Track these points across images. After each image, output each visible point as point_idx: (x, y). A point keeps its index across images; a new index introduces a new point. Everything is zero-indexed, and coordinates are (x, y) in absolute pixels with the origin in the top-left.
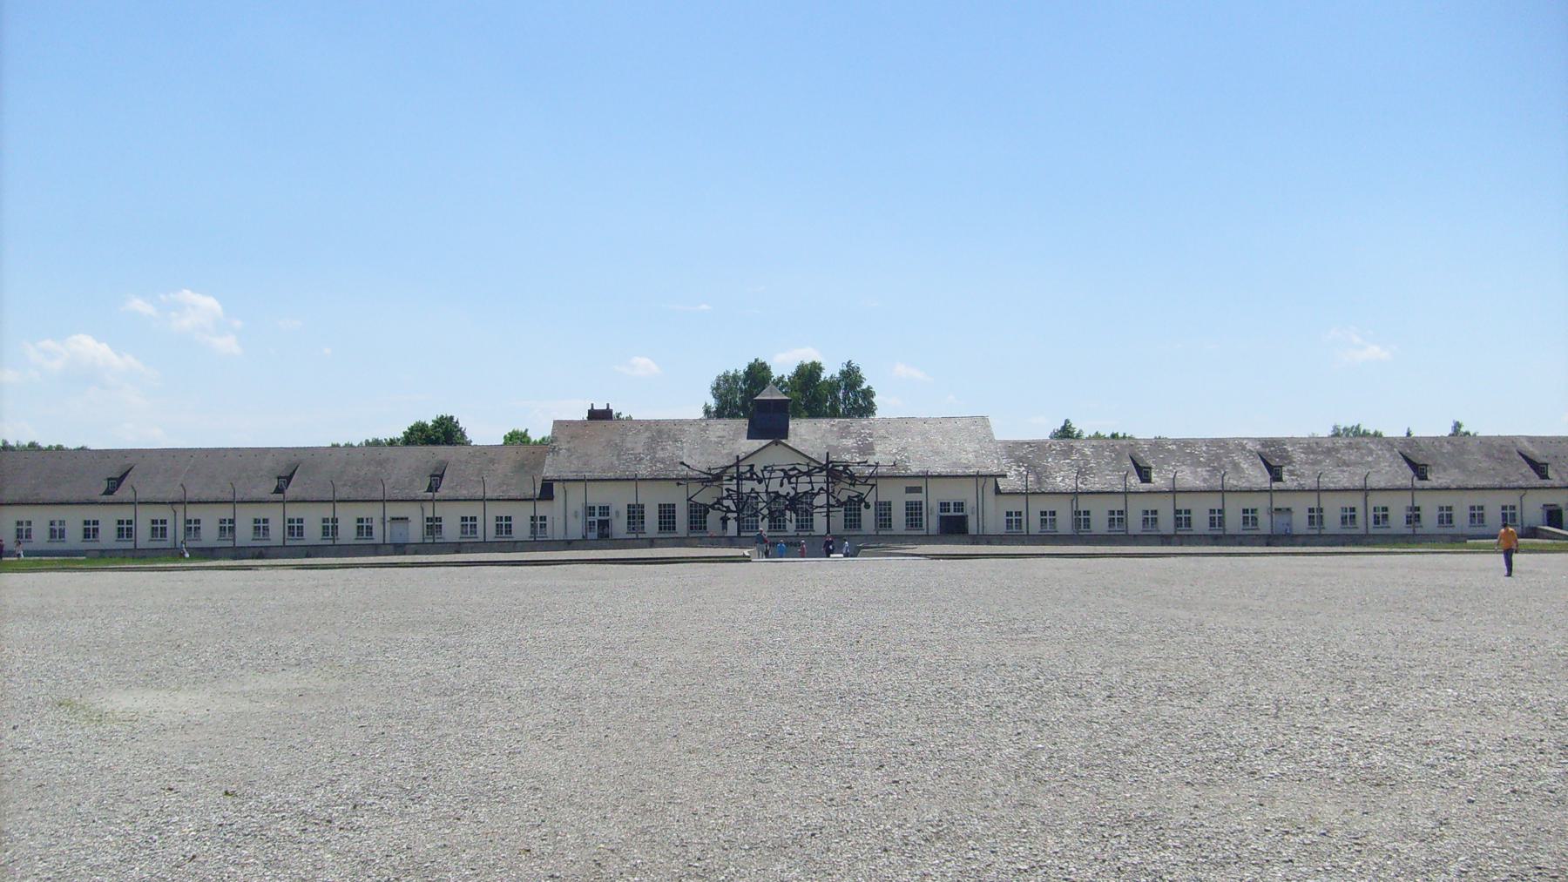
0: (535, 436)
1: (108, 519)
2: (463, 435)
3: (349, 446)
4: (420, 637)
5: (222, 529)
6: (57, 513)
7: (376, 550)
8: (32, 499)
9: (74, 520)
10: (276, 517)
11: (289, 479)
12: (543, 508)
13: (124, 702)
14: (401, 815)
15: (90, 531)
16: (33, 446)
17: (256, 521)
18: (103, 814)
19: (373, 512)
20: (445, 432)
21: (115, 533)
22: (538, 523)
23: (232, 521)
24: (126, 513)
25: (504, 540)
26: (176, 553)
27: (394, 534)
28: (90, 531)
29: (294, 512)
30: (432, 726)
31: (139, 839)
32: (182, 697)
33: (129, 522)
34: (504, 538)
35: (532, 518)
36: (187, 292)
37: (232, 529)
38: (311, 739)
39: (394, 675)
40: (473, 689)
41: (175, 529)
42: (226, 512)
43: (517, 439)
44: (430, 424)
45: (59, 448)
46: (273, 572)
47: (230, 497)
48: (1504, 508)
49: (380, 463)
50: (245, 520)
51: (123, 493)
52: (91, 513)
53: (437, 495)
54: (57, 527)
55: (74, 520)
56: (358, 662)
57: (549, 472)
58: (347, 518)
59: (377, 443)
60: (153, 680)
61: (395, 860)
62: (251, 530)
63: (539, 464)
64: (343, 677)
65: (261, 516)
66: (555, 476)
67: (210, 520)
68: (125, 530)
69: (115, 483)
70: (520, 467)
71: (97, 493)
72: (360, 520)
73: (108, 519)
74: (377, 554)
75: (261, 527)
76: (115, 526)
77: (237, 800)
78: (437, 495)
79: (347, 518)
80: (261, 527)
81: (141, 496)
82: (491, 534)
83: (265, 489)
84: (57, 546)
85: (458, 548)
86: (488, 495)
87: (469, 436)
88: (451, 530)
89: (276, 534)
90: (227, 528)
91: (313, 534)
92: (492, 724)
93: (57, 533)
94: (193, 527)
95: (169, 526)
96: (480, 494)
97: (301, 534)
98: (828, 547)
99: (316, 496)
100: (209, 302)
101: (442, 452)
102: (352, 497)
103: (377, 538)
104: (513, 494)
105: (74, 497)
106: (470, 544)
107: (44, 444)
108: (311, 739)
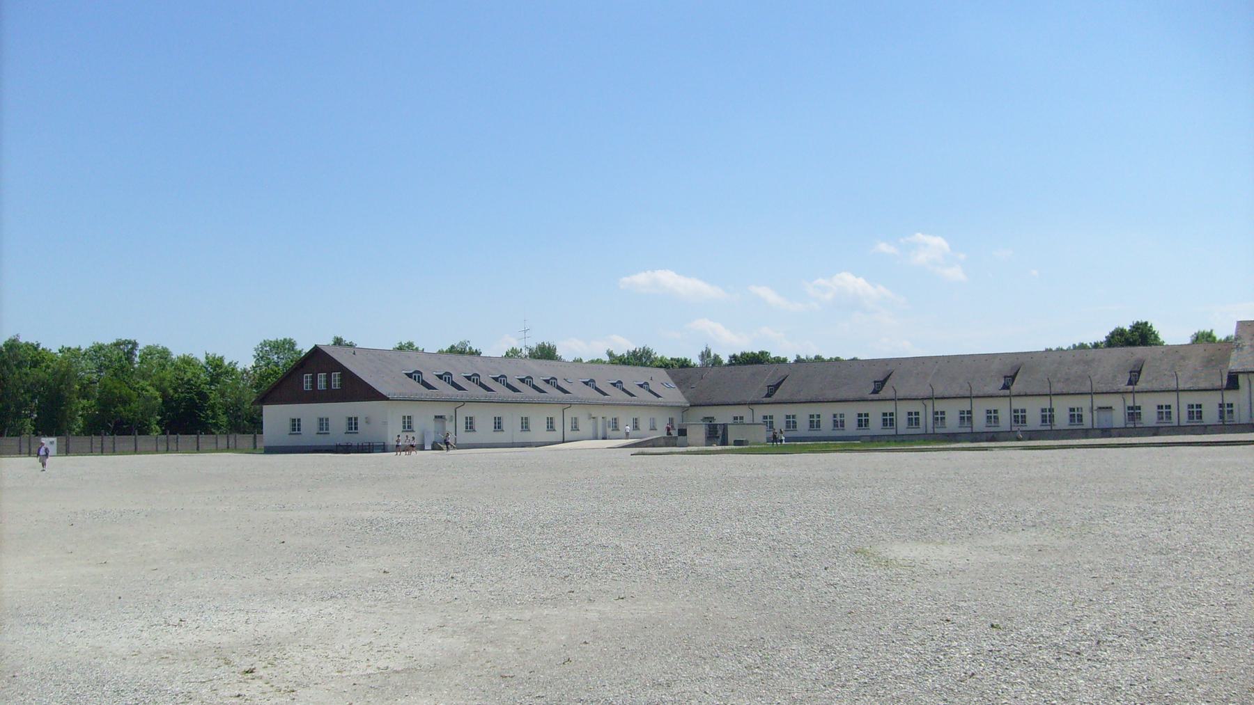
0: (1220, 335)
1: (875, 412)
2: (1156, 337)
3: (1060, 350)
4: (1132, 505)
5: (962, 419)
6: (838, 409)
7: (1086, 433)
8: (821, 398)
9: (850, 413)
10: (1004, 410)
11: (1013, 378)
12: (1230, 397)
13: (902, 551)
14: (1139, 652)
15: (863, 421)
16: (818, 358)
17: (989, 412)
18: (899, 636)
19: (1083, 403)
20: (1141, 335)
21: (808, 424)
22: (1225, 410)
23: (969, 412)
24: (889, 407)
25: (1195, 424)
26: (952, 437)
27: (1102, 420)
28: (863, 421)
29: (1018, 404)
30: (1155, 577)
31: (929, 657)
32: (946, 550)
33: (891, 414)
34: (1195, 422)
35: (1221, 406)
36: (919, 235)
37: (970, 419)
38: (1053, 586)
39: (1114, 535)
40: (1186, 550)
41: (926, 420)
42: (965, 405)
43: (1204, 338)
44: (1127, 328)
45: (837, 359)
46: (1005, 452)
47: (968, 394)
48: (835, 416)
49: (1087, 363)
50: (980, 411)
51: (886, 392)
52: (863, 408)
53: (1137, 388)
54: (838, 419)
55: (850, 413)
56: (1083, 525)
57: (1234, 366)
58: (1061, 409)
59: (1083, 346)
60: (922, 535)
61: (1139, 688)
62: (985, 418)
63: (1226, 359)
64: (1072, 537)
65: (992, 408)
66: (1240, 369)
67: (952, 412)
68: (888, 420)
69: (880, 385)
70: (1209, 362)
71: (867, 393)
72: (1072, 410)
73: (875, 412)
74: (1087, 437)
75: (992, 416)
76: (856, 418)
77: (1001, 632)
78: (1137, 388)
79: (1061, 409)
80: (992, 416)
81: (901, 394)
82: (1184, 420)
83: (995, 386)
84: (838, 433)
85: (1155, 431)
86: (1181, 387)
87: (1162, 337)
88: (1149, 416)
89: (1005, 421)
90: (966, 417)
91: (1034, 421)
92: (1206, 579)
93: (838, 423)
94: (939, 417)
95: (921, 417)
96: (1173, 385)
97: (1024, 422)
98: (222, 451)
99: (1036, 390)
100: (938, 242)
101: (1139, 351)
102: (1065, 391)
103: (1087, 423)
104: (1202, 386)
105: (852, 395)
106: (1165, 428)
107: (826, 357)
108: (1053, 586)
